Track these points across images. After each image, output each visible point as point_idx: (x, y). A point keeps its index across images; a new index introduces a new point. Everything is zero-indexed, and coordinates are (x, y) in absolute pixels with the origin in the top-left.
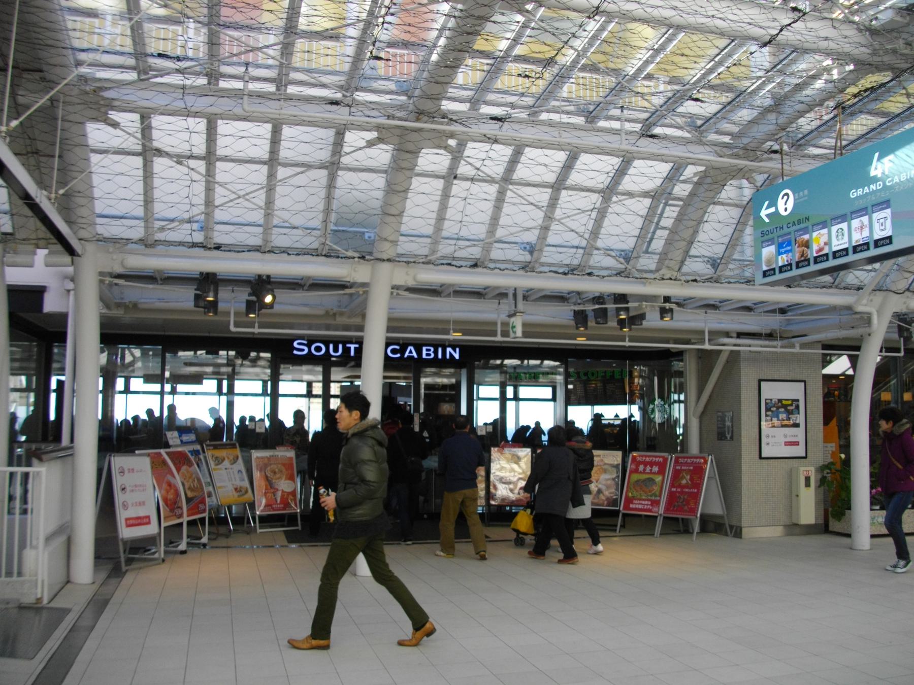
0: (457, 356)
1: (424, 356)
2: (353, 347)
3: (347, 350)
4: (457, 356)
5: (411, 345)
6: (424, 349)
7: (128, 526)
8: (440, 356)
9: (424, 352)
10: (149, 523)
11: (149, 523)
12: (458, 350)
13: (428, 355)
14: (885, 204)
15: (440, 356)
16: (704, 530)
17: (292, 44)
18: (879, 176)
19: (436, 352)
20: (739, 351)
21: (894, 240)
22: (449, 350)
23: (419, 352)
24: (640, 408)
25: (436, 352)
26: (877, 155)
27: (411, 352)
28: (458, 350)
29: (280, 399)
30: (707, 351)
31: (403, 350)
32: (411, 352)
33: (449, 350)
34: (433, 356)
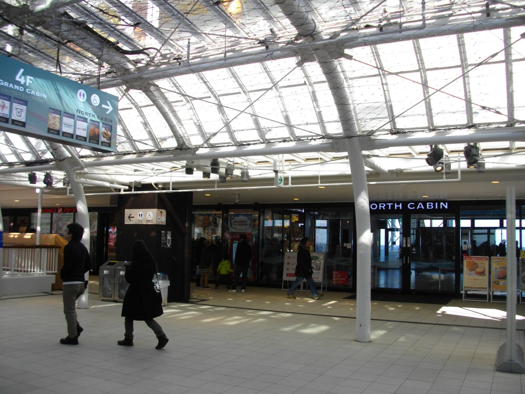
0: (446, 207)
1: (428, 208)
2: (390, 204)
3: (387, 206)
4: (446, 207)
5: (420, 202)
6: (428, 204)
7: (287, 276)
8: (437, 208)
9: (428, 206)
10: (287, 274)
11: (287, 274)
12: (447, 203)
13: (430, 207)
14: (25, 103)
15: (437, 208)
16: (285, 287)
17: (297, 26)
18: (22, 83)
19: (434, 205)
20: (191, 193)
21: (27, 126)
22: (442, 203)
23: (425, 206)
24: (400, 233)
25: (434, 205)
26: (22, 70)
27: (420, 206)
28: (447, 203)
29: (317, 230)
30: (122, 195)
31: (416, 206)
32: (420, 206)
33: (442, 203)
34: (432, 207)
